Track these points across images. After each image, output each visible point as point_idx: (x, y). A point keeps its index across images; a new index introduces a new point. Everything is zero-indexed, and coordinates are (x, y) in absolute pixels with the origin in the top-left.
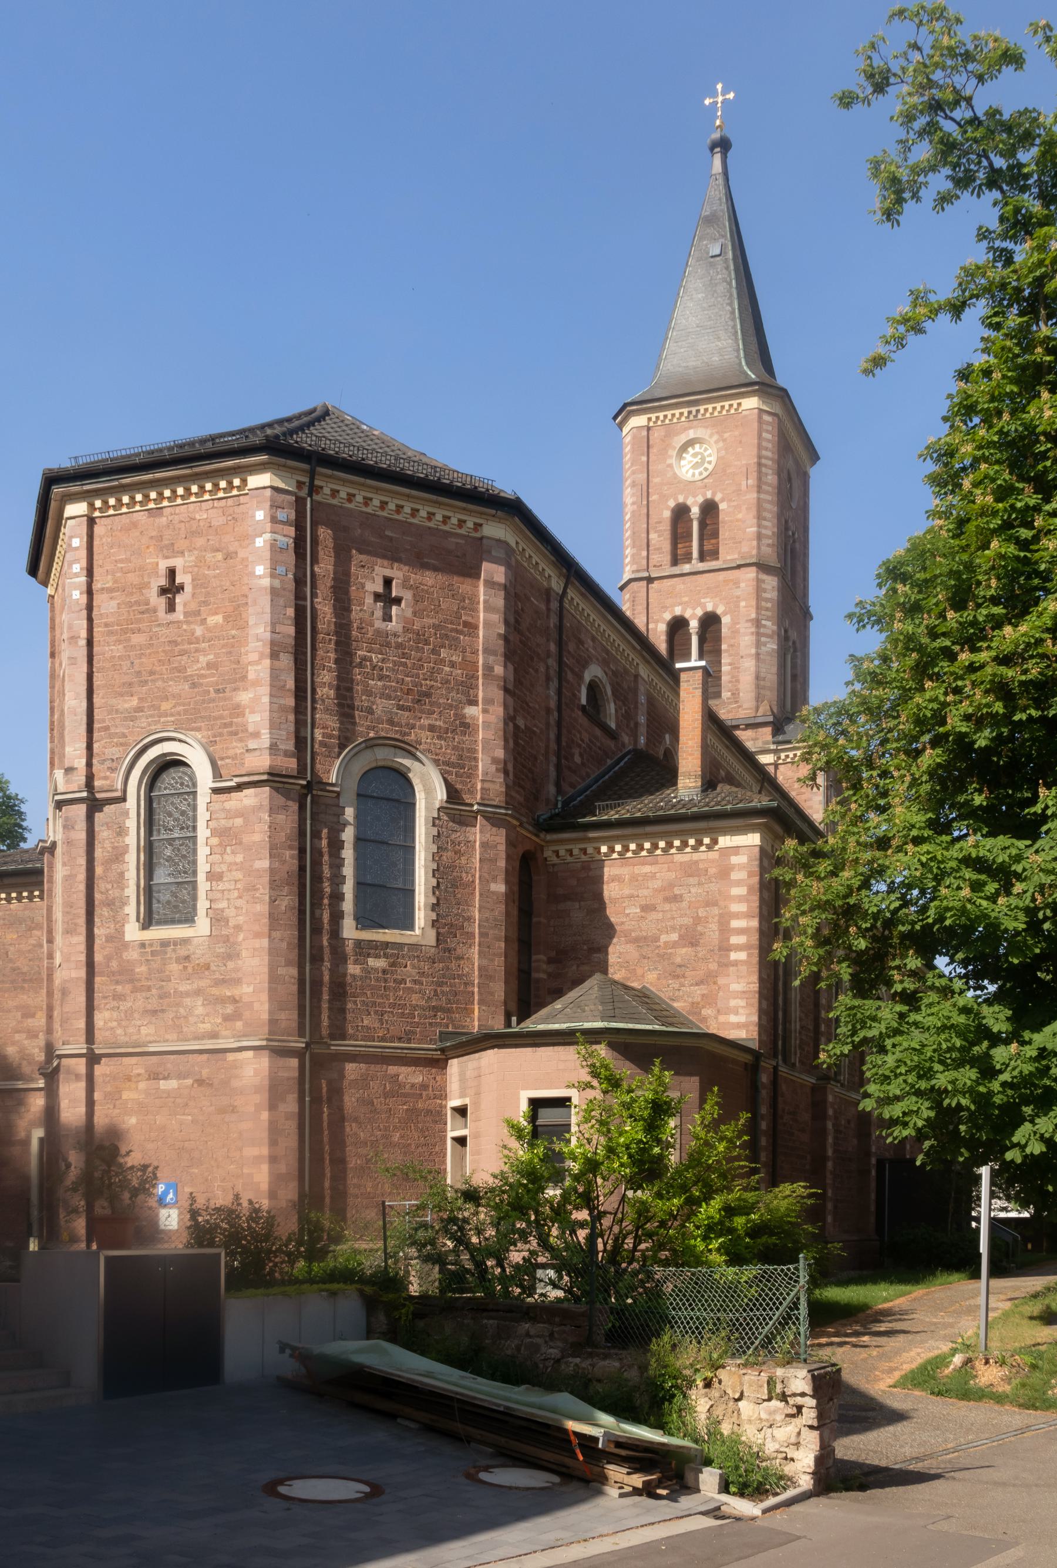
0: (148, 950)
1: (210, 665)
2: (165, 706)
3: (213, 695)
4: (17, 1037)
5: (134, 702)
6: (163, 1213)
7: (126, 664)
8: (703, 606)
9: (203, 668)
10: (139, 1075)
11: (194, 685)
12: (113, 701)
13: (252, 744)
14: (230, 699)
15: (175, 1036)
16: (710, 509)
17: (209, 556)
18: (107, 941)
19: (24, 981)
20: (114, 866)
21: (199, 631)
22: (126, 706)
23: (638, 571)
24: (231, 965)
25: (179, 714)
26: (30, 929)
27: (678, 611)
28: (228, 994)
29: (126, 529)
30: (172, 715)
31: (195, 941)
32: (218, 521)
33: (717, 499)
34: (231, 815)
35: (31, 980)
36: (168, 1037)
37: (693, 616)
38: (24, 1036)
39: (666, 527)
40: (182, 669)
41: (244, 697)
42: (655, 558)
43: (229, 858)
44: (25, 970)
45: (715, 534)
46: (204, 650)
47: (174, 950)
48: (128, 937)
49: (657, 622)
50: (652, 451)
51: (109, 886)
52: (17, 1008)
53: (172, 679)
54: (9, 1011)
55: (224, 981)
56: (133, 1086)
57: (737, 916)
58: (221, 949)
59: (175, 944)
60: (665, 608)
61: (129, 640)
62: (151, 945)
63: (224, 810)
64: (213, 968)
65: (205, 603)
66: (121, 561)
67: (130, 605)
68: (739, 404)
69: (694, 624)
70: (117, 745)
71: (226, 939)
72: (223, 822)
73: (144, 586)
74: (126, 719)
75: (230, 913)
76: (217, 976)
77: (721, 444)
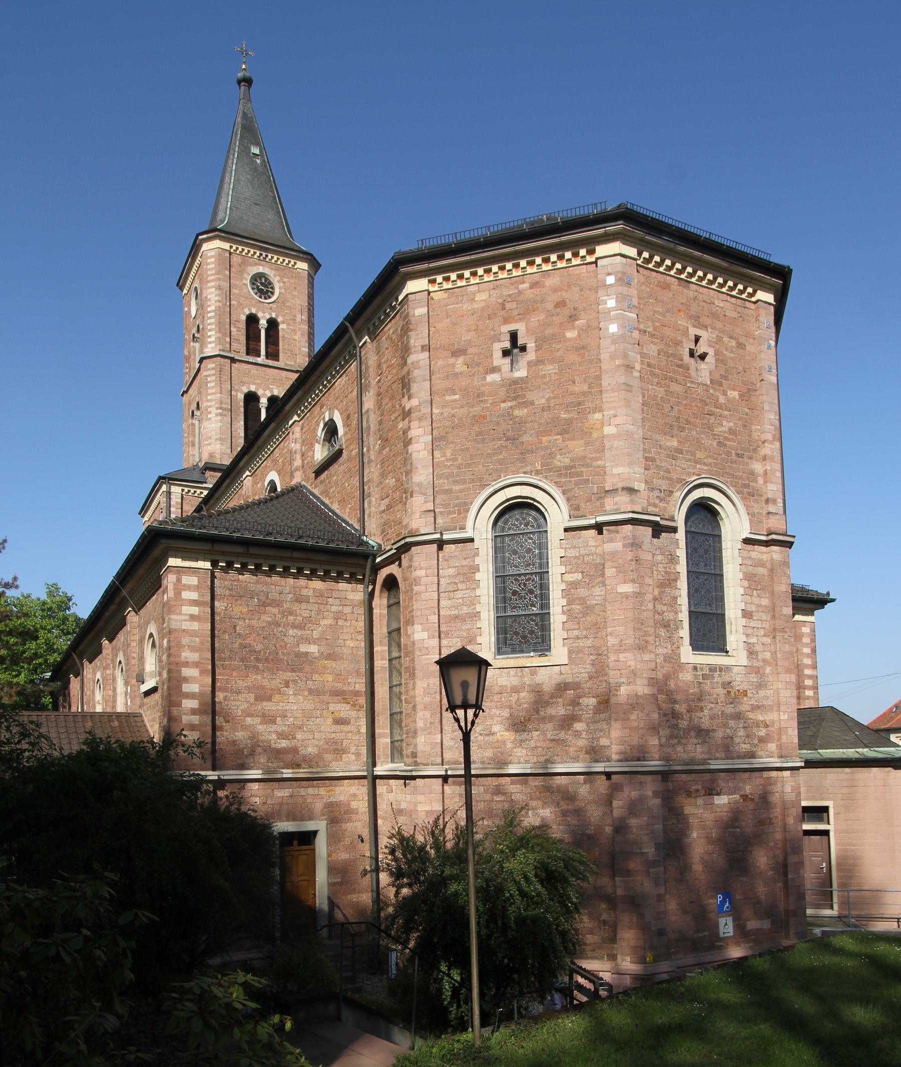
0: (699, 673)
3: (734, 457)
4: (249, 720)
8: (271, 390)
9: (725, 432)
10: (697, 790)
11: (720, 444)
12: (657, 437)
13: (771, 508)
14: (747, 464)
15: (723, 755)
17: (725, 339)
18: (665, 661)
19: (257, 660)
20: (667, 590)
21: (722, 400)
22: (668, 444)
23: (223, 351)
24: (762, 693)
25: (710, 465)
26: (264, 605)
27: (253, 388)
28: (761, 718)
30: (705, 464)
31: (735, 670)
32: (731, 314)
34: (760, 564)
35: (267, 660)
36: (718, 755)
37: (264, 395)
38: (258, 720)
39: (243, 326)
40: (710, 428)
41: (758, 467)
45: (276, 344)
46: (726, 417)
47: (720, 676)
49: (237, 391)
50: (233, 270)
51: (665, 608)
52: (249, 689)
53: (703, 433)
54: (238, 692)
55: (758, 707)
56: (693, 800)
58: (754, 678)
59: (721, 670)
60: (243, 383)
61: (669, 386)
62: (702, 669)
63: (750, 558)
64: (749, 695)
66: (658, 312)
68: (295, 263)
69: (264, 402)
70: (663, 478)
72: (751, 568)
74: (668, 456)
76: (753, 702)
77: (282, 284)
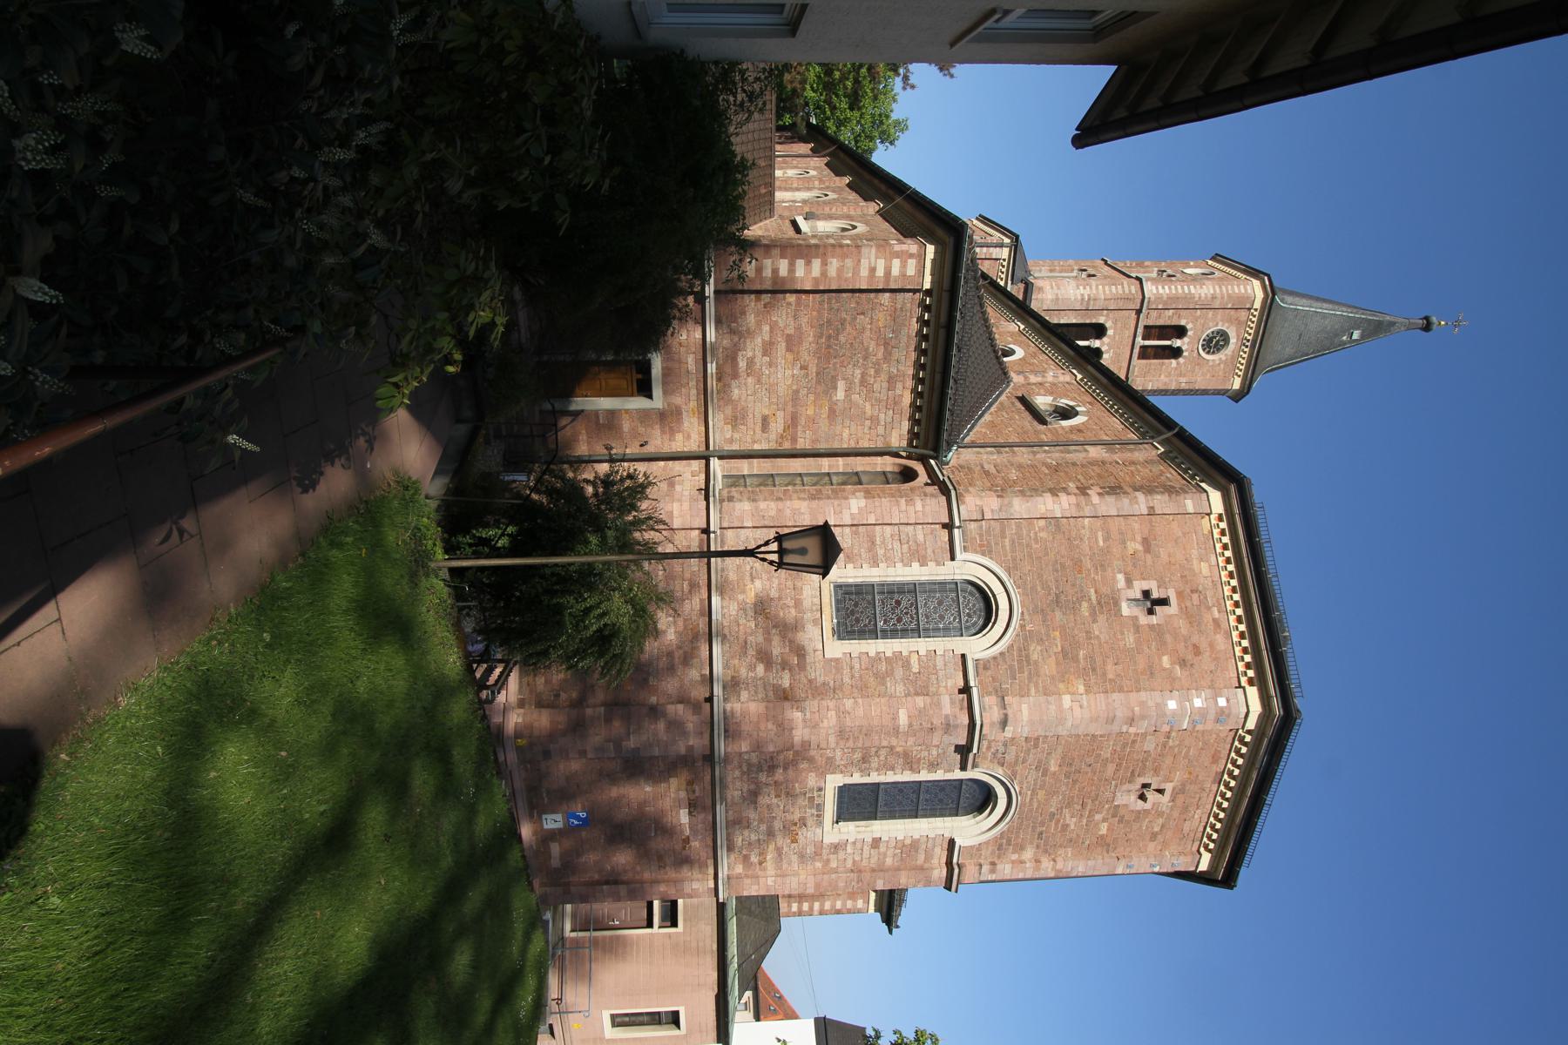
1: (1066, 826)
2: (1041, 794)
4: (766, 328)
5: (1053, 768)
6: (559, 817)
7: (1090, 760)
12: (1060, 750)
13: (986, 868)
16: (1176, 353)
17: (1161, 821)
19: (829, 337)
21: (1098, 817)
24: (795, 858)
29: (1215, 759)
31: (819, 831)
32: (1187, 827)
33: (1181, 360)
35: (829, 347)
38: (767, 338)
40: (1069, 805)
41: (1028, 854)
42: (1154, 314)
43: (890, 853)
44: (842, 338)
45: (1155, 357)
48: (829, 777)
52: (798, 328)
54: (795, 317)
55: (780, 855)
57: (904, 266)
60: (1115, 323)
65: (1120, 821)
67: (1144, 761)
69: (1096, 344)
71: (817, 854)
73: (1156, 771)
75: (841, 855)
